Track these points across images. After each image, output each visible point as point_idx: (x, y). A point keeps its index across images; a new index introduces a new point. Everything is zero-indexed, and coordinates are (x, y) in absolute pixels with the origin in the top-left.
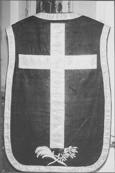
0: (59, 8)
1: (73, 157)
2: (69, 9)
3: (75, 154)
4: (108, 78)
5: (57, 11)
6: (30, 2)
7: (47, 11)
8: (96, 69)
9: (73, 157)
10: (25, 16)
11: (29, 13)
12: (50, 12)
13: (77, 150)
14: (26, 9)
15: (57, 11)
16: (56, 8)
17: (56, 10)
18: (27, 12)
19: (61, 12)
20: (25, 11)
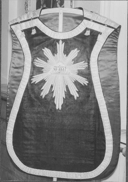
0: (61, 3)
1: (37, 59)
2: (71, 3)
3: (55, 54)
4: (71, 32)
5: (58, 5)
6: (75, 2)
7: (48, 7)
8: (25, 34)
9: (37, 59)
10: (25, 10)
11: (29, 7)
12: (51, 7)
13: (78, 50)
14: (26, 2)
15: (58, 5)
16: (57, 1)
17: (58, 4)
18: (27, 6)
19: (62, 6)
20: (25, 5)
